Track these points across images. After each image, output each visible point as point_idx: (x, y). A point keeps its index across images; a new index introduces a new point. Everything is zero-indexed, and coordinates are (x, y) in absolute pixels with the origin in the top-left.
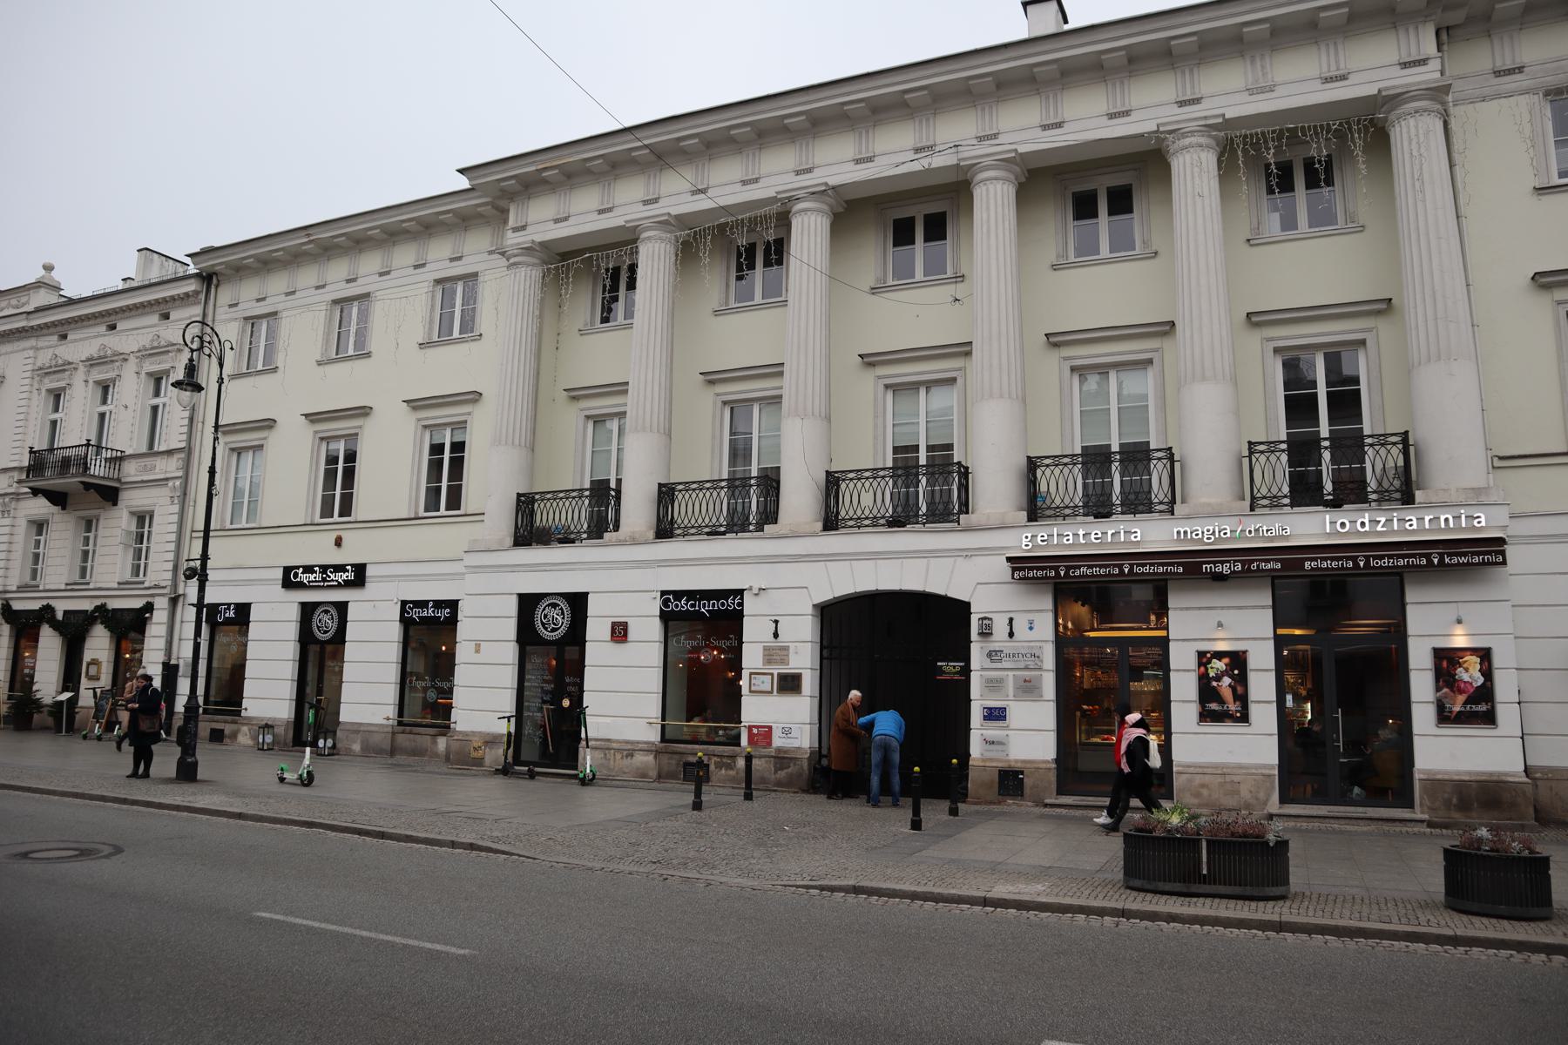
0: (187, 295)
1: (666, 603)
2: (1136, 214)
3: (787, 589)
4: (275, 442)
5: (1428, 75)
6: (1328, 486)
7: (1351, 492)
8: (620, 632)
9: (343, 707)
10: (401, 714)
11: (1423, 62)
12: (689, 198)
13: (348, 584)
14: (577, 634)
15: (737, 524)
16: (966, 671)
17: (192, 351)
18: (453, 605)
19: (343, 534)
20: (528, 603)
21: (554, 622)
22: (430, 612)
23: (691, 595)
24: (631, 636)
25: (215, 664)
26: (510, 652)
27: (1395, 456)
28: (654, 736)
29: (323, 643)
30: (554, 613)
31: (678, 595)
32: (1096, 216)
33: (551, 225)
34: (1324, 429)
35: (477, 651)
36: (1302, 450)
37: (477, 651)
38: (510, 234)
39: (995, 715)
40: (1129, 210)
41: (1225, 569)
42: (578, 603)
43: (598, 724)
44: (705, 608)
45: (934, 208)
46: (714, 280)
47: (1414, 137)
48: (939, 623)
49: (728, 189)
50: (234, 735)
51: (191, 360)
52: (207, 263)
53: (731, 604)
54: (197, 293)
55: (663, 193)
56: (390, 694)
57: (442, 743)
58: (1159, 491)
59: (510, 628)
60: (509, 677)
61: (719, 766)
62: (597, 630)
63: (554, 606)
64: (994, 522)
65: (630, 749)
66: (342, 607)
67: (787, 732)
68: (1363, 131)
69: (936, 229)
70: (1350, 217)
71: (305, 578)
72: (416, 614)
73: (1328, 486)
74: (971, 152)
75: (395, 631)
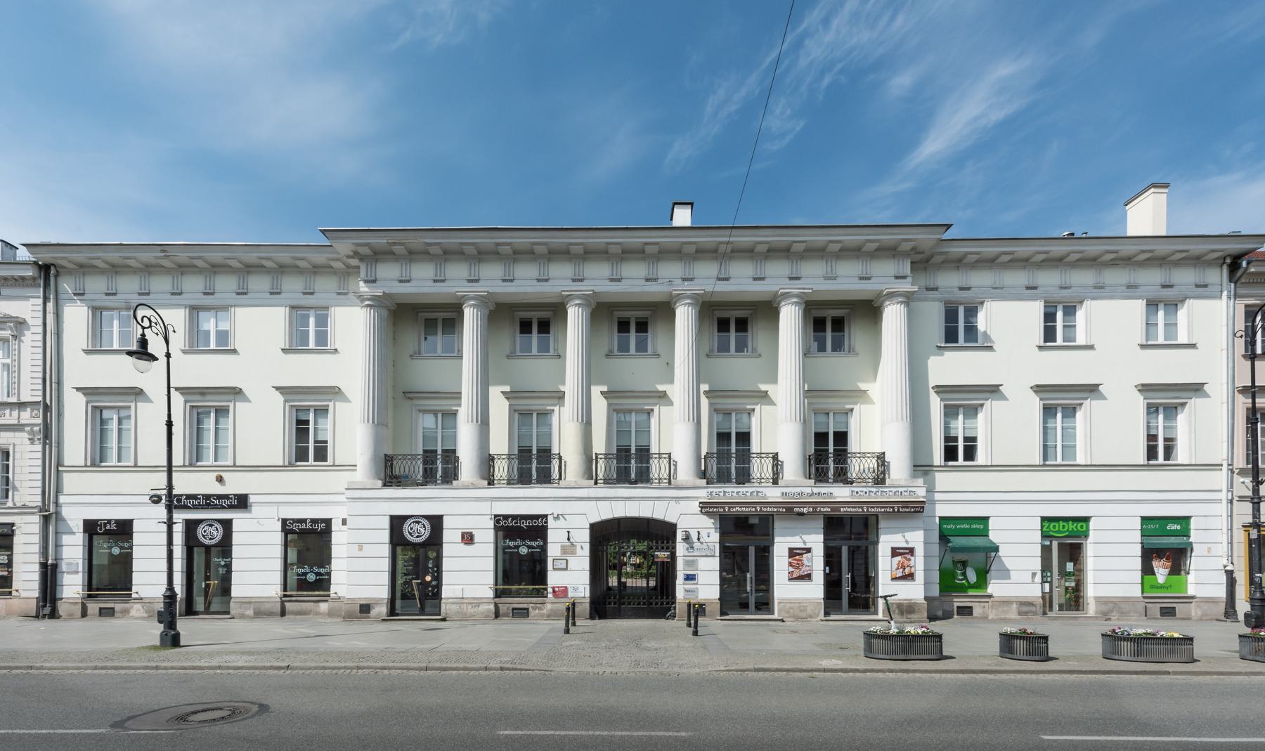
0: (23, 278)
1: (498, 521)
2: (650, 334)
3: (572, 513)
4: (339, 409)
5: (906, 286)
6: (633, 476)
7: (842, 476)
8: (468, 538)
9: (233, 588)
10: (285, 590)
11: (904, 277)
12: (500, 283)
13: (231, 507)
14: (435, 539)
15: (429, 478)
16: (673, 556)
17: (143, 328)
18: (328, 522)
19: (223, 474)
20: (397, 523)
21: (420, 533)
22: (309, 526)
23: (514, 517)
24: (476, 540)
25: (95, 562)
26: (385, 550)
27: (769, 463)
28: (491, 594)
29: (208, 548)
30: (418, 527)
31: (506, 517)
32: (728, 331)
33: (397, 284)
34: (831, 448)
35: (360, 549)
36: (723, 456)
37: (360, 549)
38: (362, 284)
39: (690, 578)
40: (746, 331)
41: (804, 510)
42: (436, 522)
43: (450, 590)
44: (524, 524)
45: (543, 315)
46: (610, 337)
47: (893, 317)
48: (659, 534)
49: (529, 283)
50: (126, 612)
51: (143, 335)
52: (45, 257)
53: (540, 522)
54: (34, 279)
55: (413, 276)
56: (277, 578)
57: (324, 607)
58: (555, 475)
59: (385, 536)
60: (385, 564)
61: (534, 609)
62: (450, 537)
63: (418, 522)
64: (573, 484)
65: (477, 602)
66: (227, 525)
67: (575, 589)
68: (870, 310)
69: (544, 327)
70: (754, 350)
71: (189, 503)
72: (296, 527)
73: (633, 476)
74: (680, 287)
75: (278, 537)
